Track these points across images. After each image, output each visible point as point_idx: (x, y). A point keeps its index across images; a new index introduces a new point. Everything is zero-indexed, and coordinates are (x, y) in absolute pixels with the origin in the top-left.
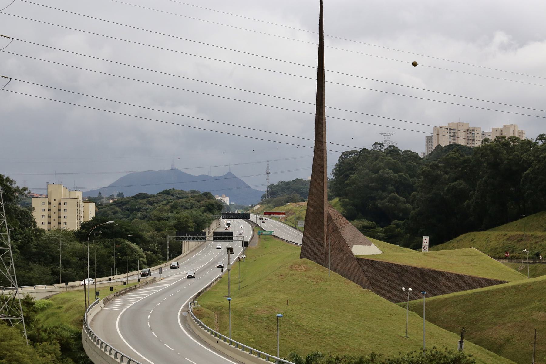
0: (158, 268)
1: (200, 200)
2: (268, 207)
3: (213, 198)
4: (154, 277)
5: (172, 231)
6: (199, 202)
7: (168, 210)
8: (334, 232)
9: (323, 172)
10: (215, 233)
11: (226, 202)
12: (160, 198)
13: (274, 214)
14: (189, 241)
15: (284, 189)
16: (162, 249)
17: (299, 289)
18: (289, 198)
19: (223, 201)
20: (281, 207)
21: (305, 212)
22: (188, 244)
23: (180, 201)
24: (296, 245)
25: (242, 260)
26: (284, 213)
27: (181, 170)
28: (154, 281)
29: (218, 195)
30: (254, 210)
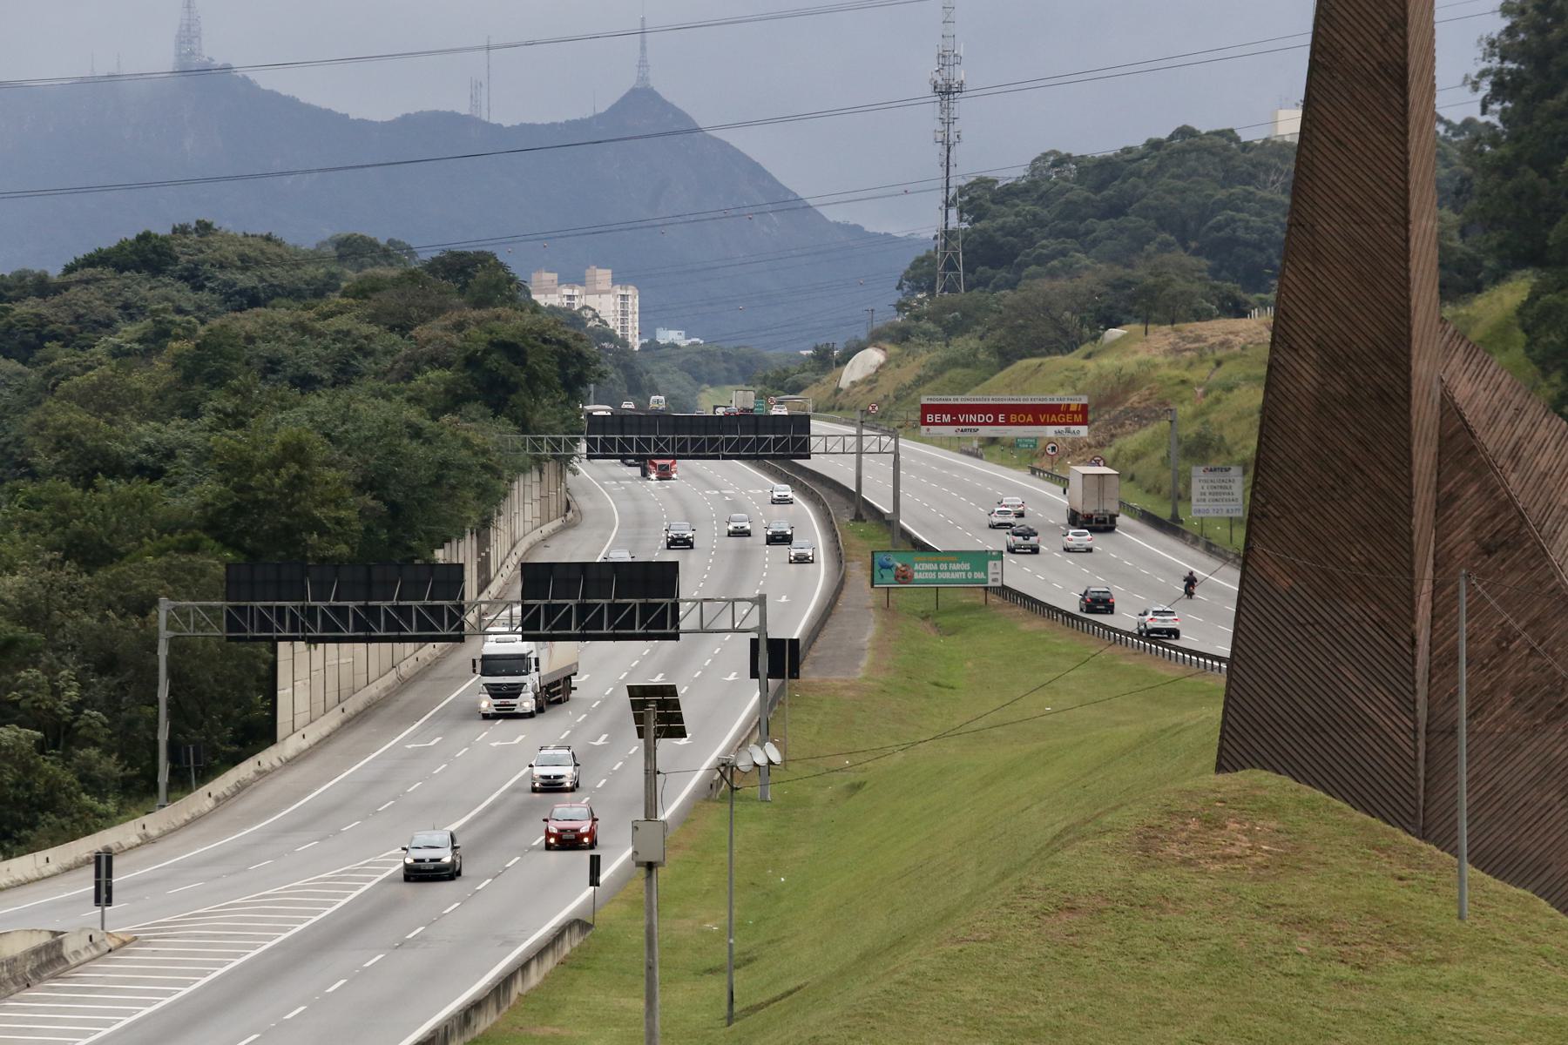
0: (87, 862)
1: (414, 312)
2: (952, 363)
3: (512, 299)
4: (55, 934)
5: (198, 560)
6: (403, 328)
7: (160, 397)
8: (1499, 555)
9: (1404, 67)
10: (536, 577)
11: (614, 324)
12: (87, 298)
13: (1001, 417)
14: (324, 640)
15: (1083, 219)
16: (112, 706)
17: (1216, 1020)
18: (1120, 285)
19: (596, 316)
20: (1060, 360)
21: (1252, 397)
22: (318, 662)
23: (248, 321)
24: (1180, 667)
25: (751, 789)
26: (1085, 407)
27: (252, 75)
28: (50, 963)
29: (555, 276)
30: (838, 390)
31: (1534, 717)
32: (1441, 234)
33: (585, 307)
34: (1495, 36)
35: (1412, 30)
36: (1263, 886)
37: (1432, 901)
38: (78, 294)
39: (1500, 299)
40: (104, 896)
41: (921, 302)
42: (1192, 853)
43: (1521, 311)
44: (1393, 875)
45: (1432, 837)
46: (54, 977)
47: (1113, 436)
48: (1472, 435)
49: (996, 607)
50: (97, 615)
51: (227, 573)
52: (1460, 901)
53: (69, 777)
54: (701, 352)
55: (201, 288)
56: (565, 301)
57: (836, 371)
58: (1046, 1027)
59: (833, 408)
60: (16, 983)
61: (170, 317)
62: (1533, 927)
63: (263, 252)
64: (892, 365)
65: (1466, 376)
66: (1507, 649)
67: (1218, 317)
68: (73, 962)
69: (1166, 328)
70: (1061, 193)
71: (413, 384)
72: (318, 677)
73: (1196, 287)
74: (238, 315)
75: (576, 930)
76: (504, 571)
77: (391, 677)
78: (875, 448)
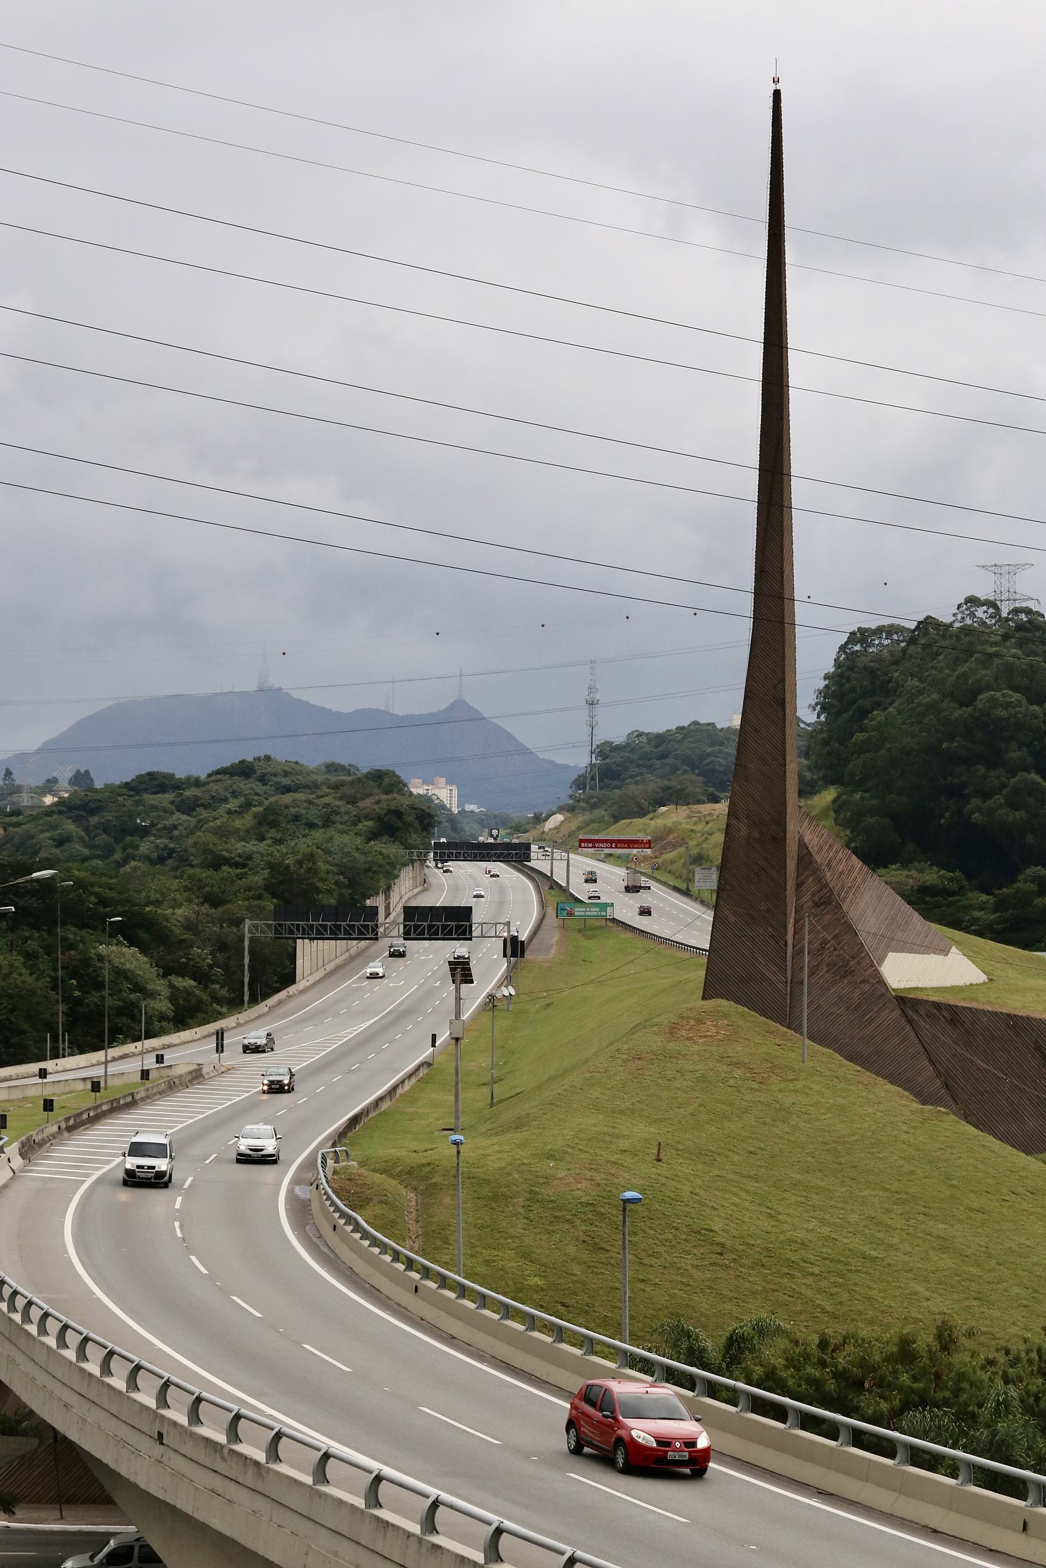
0: (213, 1034)
2: (593, 821)
4: (199, 1065)
5: (262, 903)
6: (353, 801)
7: (247, 831)
8: (822, 907)
10: (410, 912)
11: (447, 802)
15: (650, 759)
17: (700, 1106)
21: (720, 838)
22: (314, 949)
23: (287, 799)
26: (649, 841)
28: (197, 1077)
29: (421, 780)
31: (835, 976)
32: (799, 771)
33: (434, 794)
34: (821, 688)
35: (787, 683)
36: (721, 1049)
37: (791, 1054)
38: (213, 786)
39: (824, 798)
40: (220, 1049)
41: (580, 794)
42: (691, 1035)
43: (834, 801)
44: (776, 1044)
45: (793, 1027)
46: (199, 1084)
47: (661, 854)
48: (811, 856)
49: (611, 927)
50: (218, 926)
51: (275, 909)
52: (803, 1055)
53: (205, 997)
54: (485, 815)
55: (267, 784)
56: (425, 791)
57: (543, 823)
58: (628, 1108)
59: (541, 840)
60: (182, 1086)
61: (253, 797)
62: (833, 1065)
63: (293, 769)
64: (567, 821)
65: (810, 830)
66: (825, 947)
67: (707, 803)
68: (206, 1077)
69: (685, 807)
70: (641, 748)
71: (357, 827)
72: (314, 955)
73: (698, 790)
74: (282, 796)
75: (425, 1066)
76: (396, 909)
77: (346, 956)
78: (559, 858)
